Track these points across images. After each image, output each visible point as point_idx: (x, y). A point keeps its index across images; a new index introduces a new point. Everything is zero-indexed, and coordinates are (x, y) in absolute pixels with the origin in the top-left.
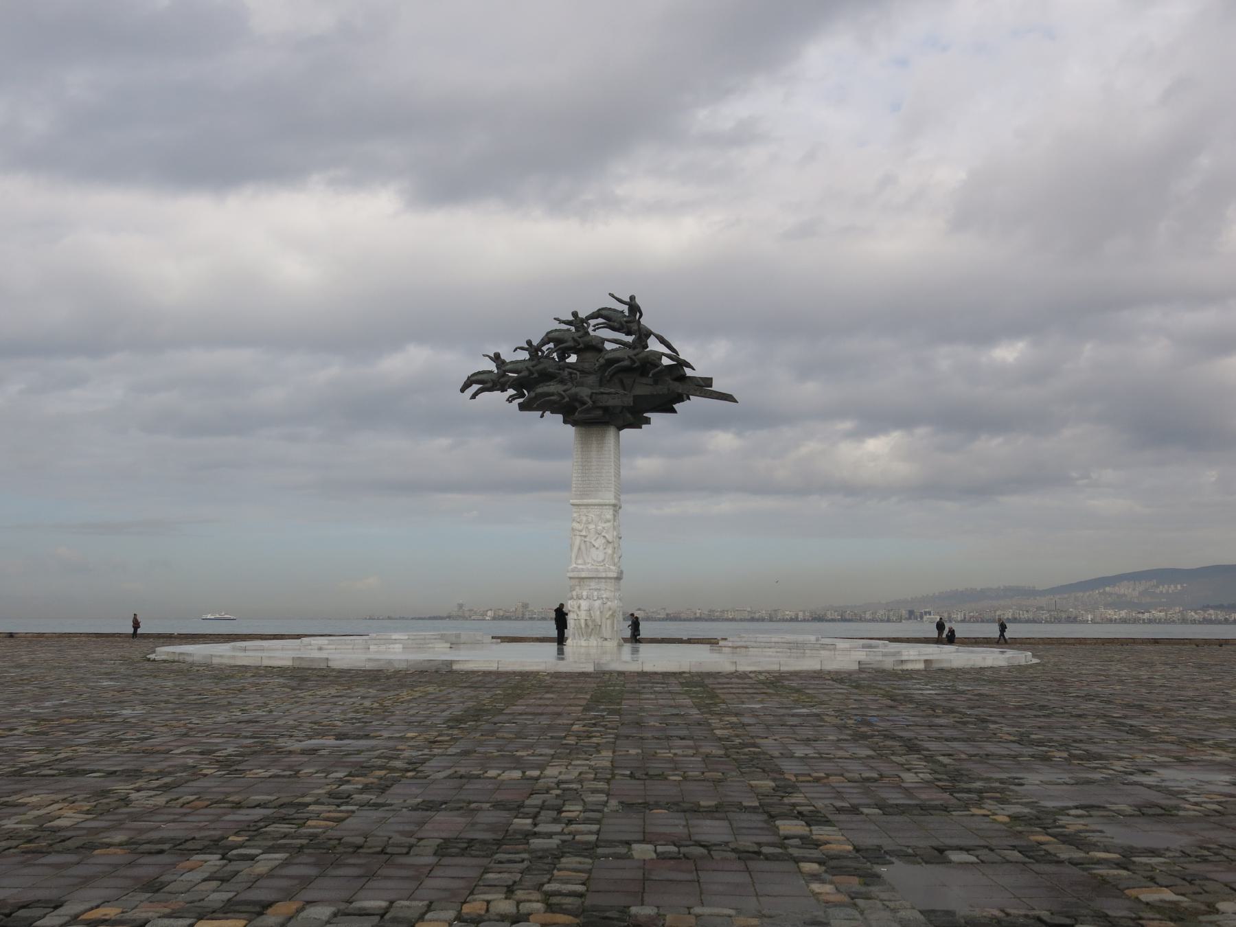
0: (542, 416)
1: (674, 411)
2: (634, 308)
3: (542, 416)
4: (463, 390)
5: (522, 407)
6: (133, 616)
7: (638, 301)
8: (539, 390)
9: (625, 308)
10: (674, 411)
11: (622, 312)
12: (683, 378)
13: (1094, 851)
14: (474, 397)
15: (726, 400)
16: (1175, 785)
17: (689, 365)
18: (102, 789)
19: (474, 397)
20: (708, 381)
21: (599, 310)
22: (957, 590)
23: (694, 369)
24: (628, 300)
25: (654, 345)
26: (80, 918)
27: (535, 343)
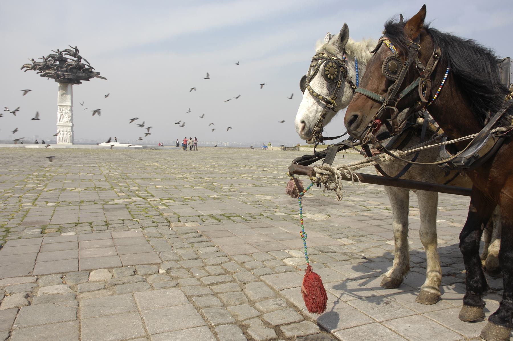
0: (48, 79)
1: (89, 80)
2: (77, 50)
3: (48, 79)
4: (21, 69)
5: (41, 76)
7: (78, 48)
9: (74, 50)
10: (89, 80)
12: (92, 72)
14: (25, 71)
17: (93, 68)
19: (25, 71)
20: (99, 73)
21: (66, 50)
24: (75, 48)
25: (83, 62)
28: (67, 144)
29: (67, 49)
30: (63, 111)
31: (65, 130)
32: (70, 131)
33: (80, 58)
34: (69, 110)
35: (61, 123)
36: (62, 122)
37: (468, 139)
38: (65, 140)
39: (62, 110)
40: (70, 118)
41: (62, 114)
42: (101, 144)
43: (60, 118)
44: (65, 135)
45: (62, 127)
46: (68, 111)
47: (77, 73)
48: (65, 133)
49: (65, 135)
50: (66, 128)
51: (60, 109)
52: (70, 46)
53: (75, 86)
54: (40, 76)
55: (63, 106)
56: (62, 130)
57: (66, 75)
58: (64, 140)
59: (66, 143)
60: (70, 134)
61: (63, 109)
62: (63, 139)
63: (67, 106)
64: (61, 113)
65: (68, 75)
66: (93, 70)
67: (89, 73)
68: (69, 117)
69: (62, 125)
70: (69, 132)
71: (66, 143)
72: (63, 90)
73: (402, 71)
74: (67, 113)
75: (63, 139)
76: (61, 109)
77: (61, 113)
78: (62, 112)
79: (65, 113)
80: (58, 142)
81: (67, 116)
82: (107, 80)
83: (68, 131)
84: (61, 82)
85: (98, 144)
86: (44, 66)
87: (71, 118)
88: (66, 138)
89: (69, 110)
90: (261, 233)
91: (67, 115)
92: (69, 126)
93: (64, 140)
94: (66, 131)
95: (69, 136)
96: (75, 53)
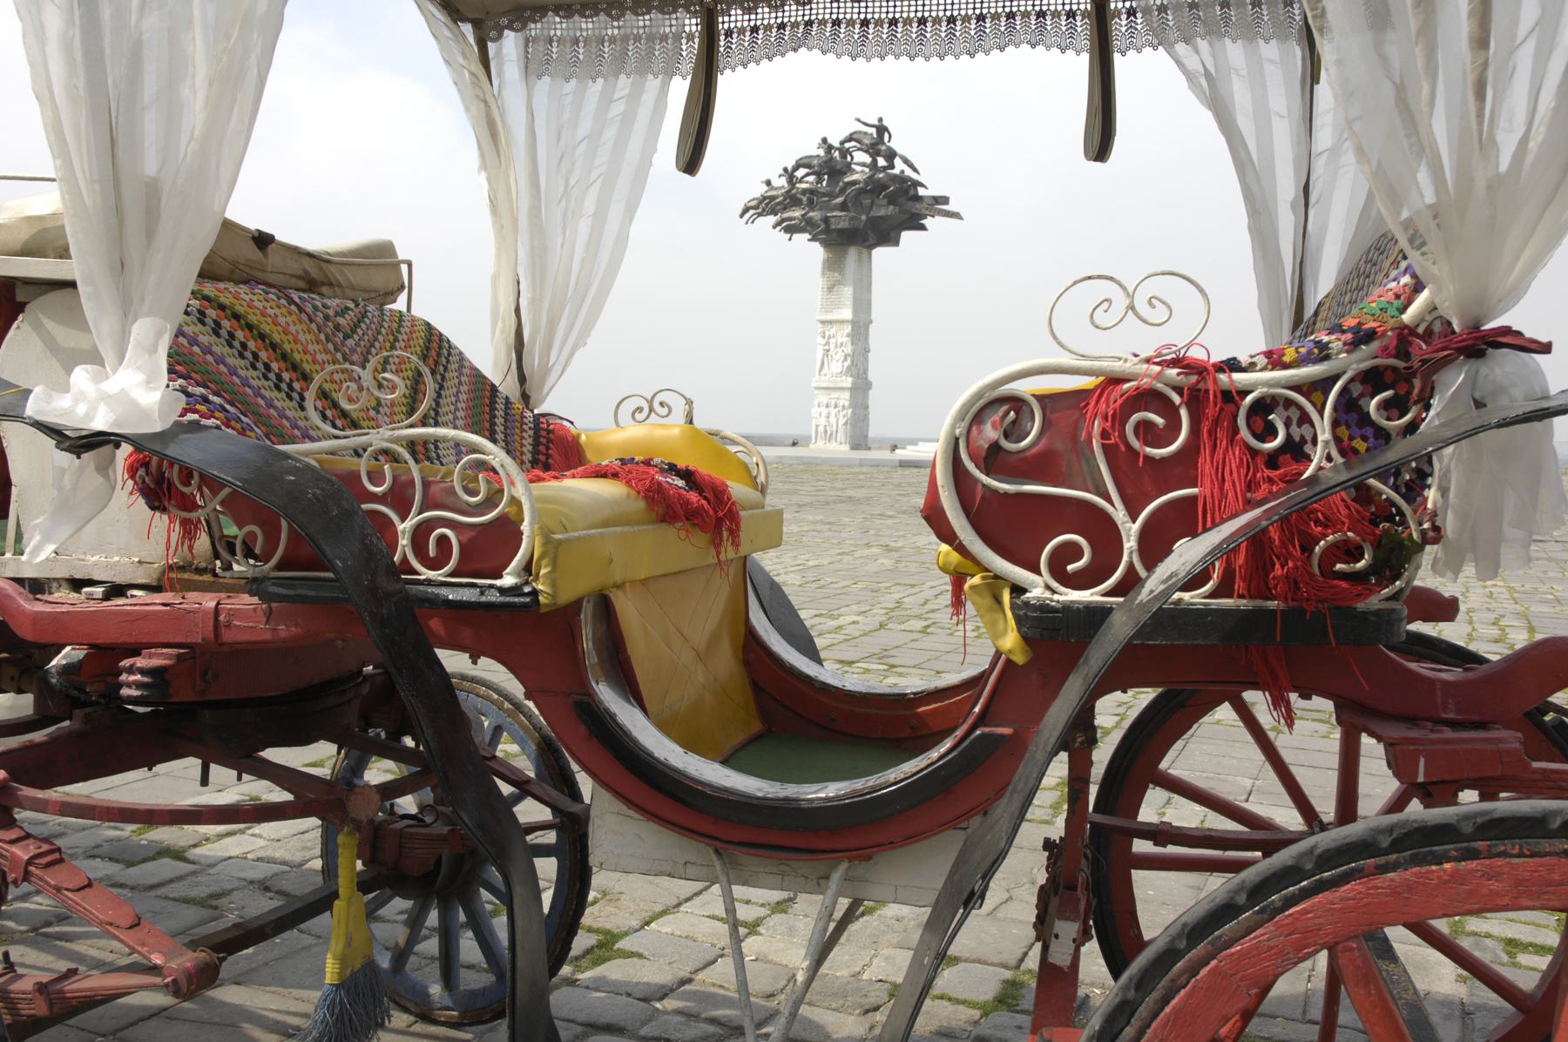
0: (790, 239)
1: (923, 228)
2: (882, 129)
3: (790, 239)
6: (1544, 339)
7: (885, 123)
8: (785, 215)
9: (873, 131)
10: (923, 228)
11: (872, 134)
12: (918, 198)
13: (33, 520)
15: (951, 216)
16: (461, 590)
17: (922, 185)
18: (871, 862)
20: (945, 200)
21: (851, 135)
22: (687, 467)
23: (926, 187)
24: (876, 123)
26: (306, 866)
27: (790, 168)
28: (836, 448)
29: (855, 133)
30: (832, 341)
31: (833, 402)
32: (847, 404)
33: (891, 156)
34: (848, 336)
35: (823, 378)
36: (825, 375)
37: (924, 775)
38: (831, 435)
39: (829, 337)
40: (849, 360)
41: (828, 351)
42: (904, 448)
43: (823, 363)
44: (833, 419)
45: (828, 392)
46: (845, 339)
47: (874, 209)
48: (833, 411)
49: (833, 419)
50: (836, 396)
51: (824, 333)
52: (859, 120)
53: (880, 254)
54: (951, 201)
55: (831, 322)
56: (825, 402)
57: (833, 220)
58: (829, 433)
59: (833, 446)
60: (844, 416)
61: (833, 331)
62: (826, 432)
63: (841, 322)
64: (825, 345)
65: (841, 219)
66: (921, 191)
67: (910, 203)
68: (845, 359)
69: (825, 385)
70: (844, 407)
71: (833, 446)
72: (834, 271)
73: (220, 348)
74: (842, 344)
75: (826, 432)
76: (827, 333)
77: (825, 345)
78: (827, 343)
79: (836, 346)
80: (813, 441)
81: (840, 356)
82: (962, 219)
83: (841, 404)
84: (826, 244)
85: (894, 448)
86: (784, 200)
87: (852, 362)
88: (834, 428)
89: (848, 336)
90: (654, 1023)
91: (839, 350)
92: (842, 389)
93: (829, 433)
94: (836, 407)
95: (842, 421)
96: (877, 141)
